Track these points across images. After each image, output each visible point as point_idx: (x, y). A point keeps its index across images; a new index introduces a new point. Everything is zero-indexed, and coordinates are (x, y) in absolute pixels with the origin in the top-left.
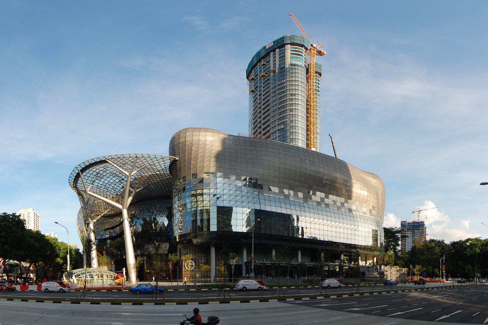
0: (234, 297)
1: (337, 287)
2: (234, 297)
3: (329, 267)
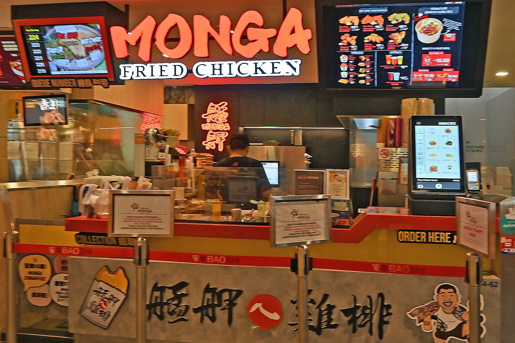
0: (108, 105)
1: (186, 309)
2: (108, 105)
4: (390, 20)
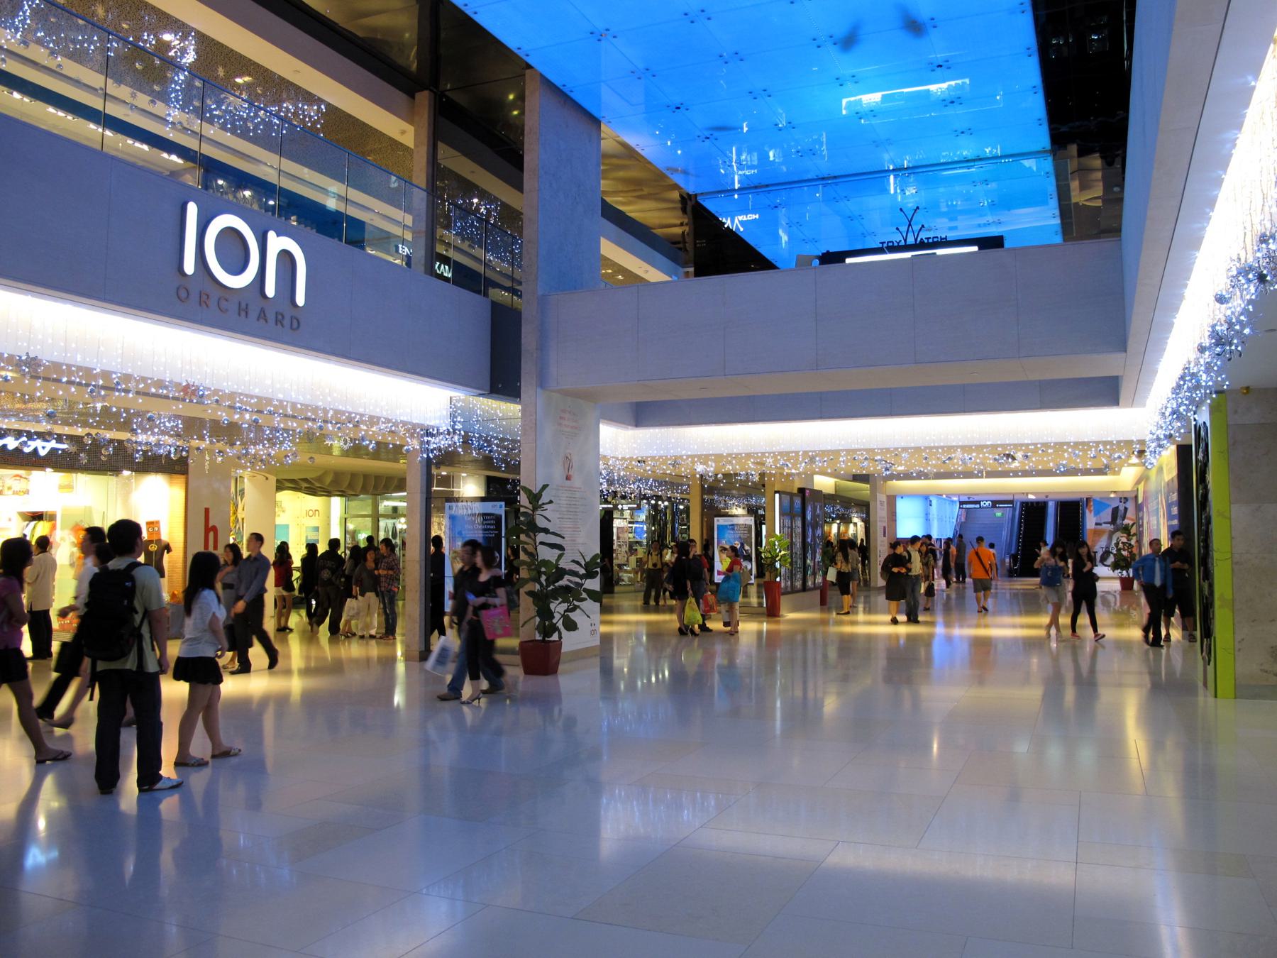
0: (1006, 505)
3: (513, 105)
4: (418, 95)
